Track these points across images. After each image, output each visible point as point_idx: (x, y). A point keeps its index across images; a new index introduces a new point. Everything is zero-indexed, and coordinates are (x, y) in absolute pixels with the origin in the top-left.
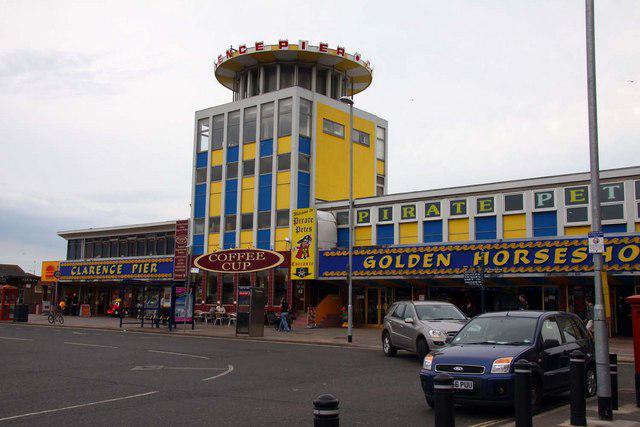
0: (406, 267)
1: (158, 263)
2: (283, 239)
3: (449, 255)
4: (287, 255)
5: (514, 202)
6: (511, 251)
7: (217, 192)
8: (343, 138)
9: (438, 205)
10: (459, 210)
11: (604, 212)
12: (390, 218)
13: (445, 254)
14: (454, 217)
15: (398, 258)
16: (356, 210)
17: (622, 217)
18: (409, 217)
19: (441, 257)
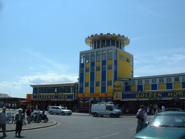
0: (149, 97)
1: (67, 95)
3: (161, 94)
8: (124, 60)
9: (156, 80)
10: (162, 81)
12: (141, 83)
13: (160, 93)
14: (160, 83)
15: (146, 95)
16: (131, 81)
18: (147, 83)
19: (159, 94)
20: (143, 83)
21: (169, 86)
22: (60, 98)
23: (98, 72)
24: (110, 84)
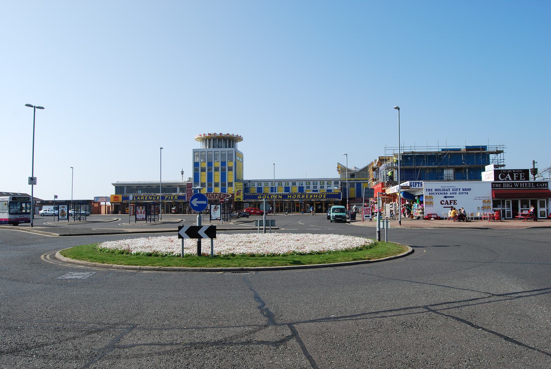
2: (231, 190)
4: (233, 195)
5: (294, 184)
6: (323, 195)
7: (204, 177)
11: (314, 187)
17: (218, 183)
20: (263, 185)
21: (287, 189)
22: (167, 199)
23: (216, 173)
24: (230, 184)
